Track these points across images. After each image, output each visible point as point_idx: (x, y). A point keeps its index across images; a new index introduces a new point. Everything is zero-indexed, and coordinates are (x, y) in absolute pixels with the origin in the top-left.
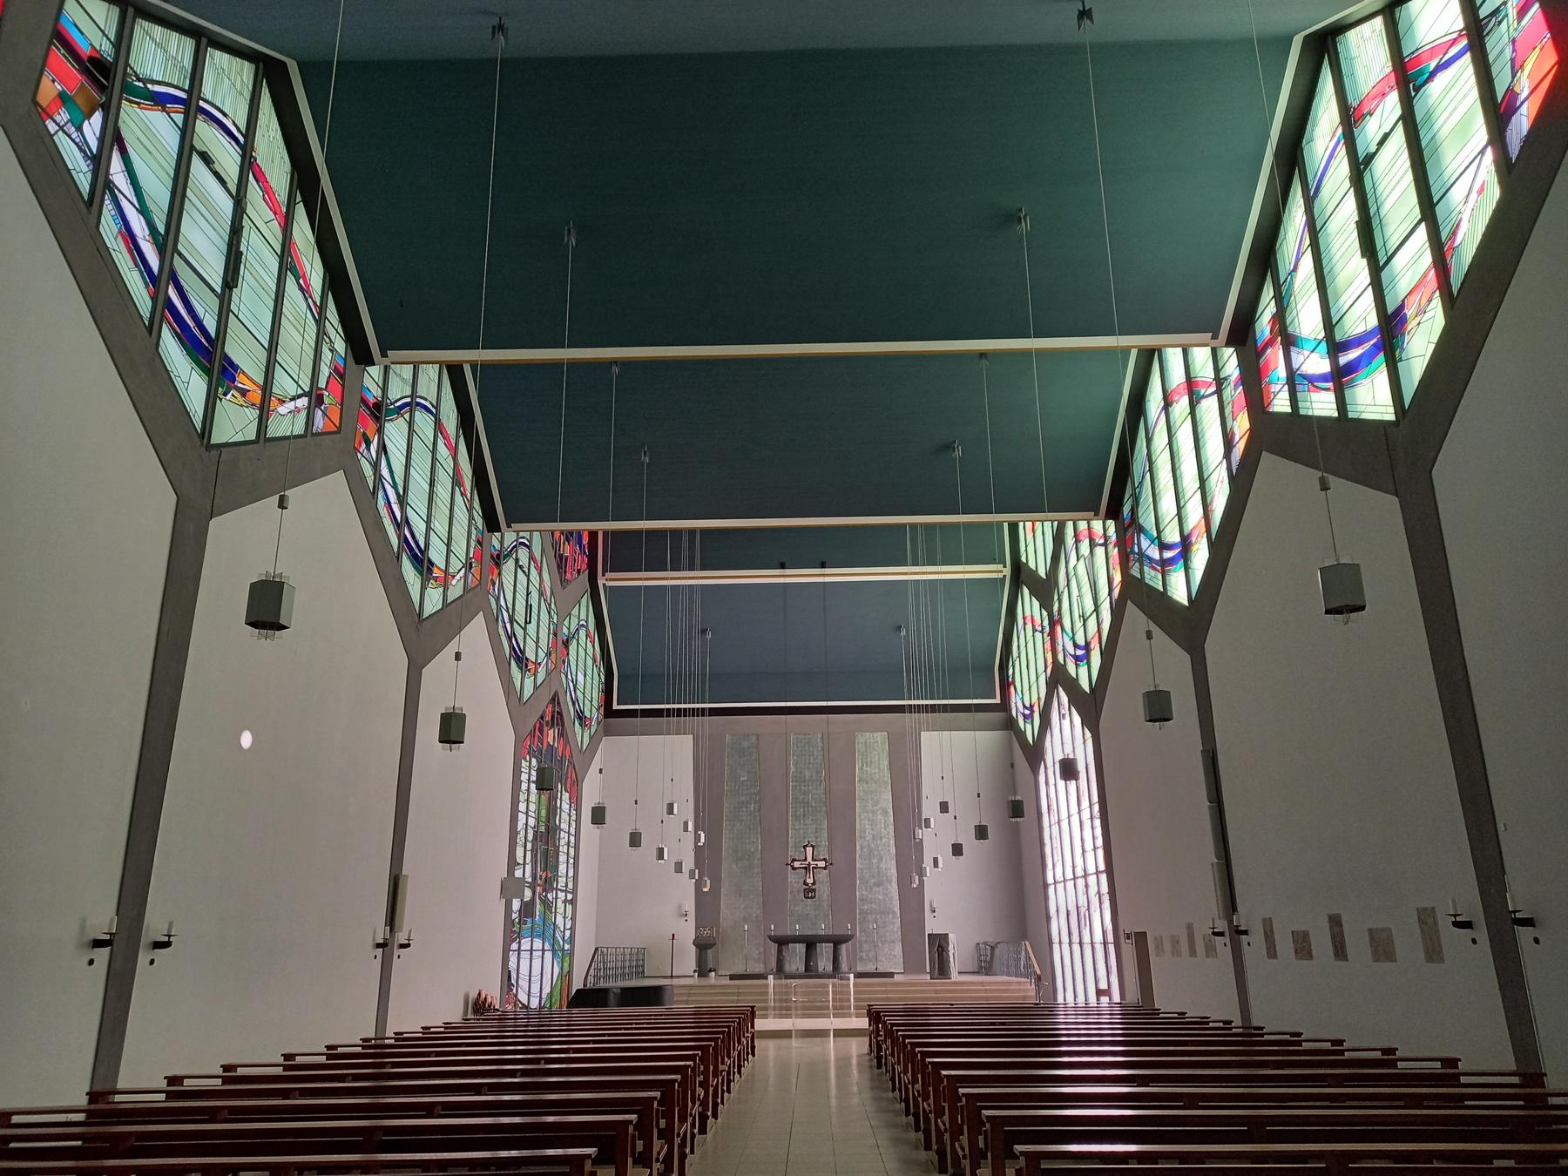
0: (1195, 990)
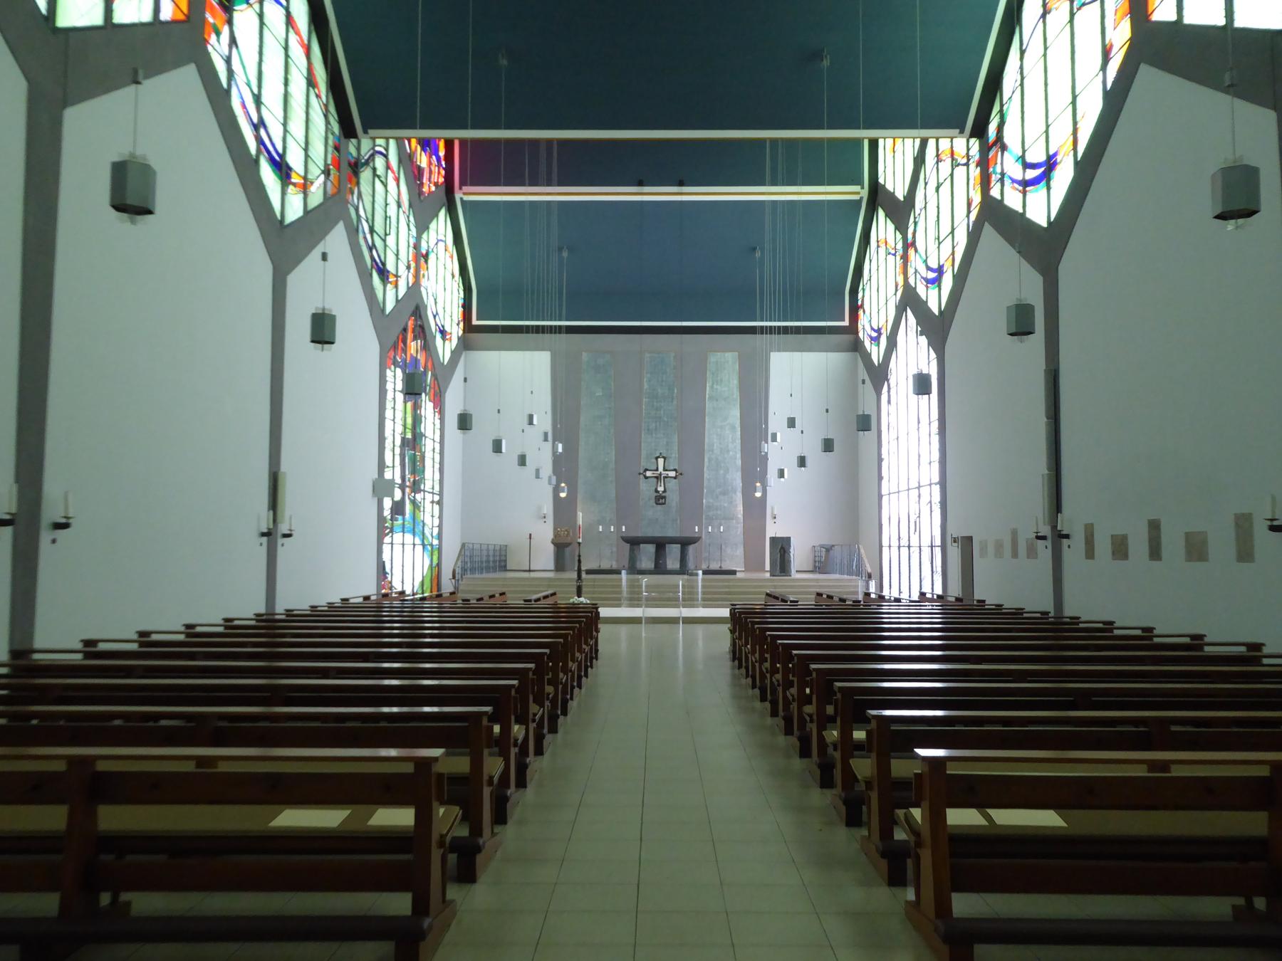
0: (1011, 585)
